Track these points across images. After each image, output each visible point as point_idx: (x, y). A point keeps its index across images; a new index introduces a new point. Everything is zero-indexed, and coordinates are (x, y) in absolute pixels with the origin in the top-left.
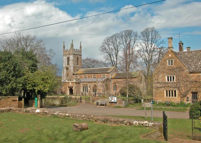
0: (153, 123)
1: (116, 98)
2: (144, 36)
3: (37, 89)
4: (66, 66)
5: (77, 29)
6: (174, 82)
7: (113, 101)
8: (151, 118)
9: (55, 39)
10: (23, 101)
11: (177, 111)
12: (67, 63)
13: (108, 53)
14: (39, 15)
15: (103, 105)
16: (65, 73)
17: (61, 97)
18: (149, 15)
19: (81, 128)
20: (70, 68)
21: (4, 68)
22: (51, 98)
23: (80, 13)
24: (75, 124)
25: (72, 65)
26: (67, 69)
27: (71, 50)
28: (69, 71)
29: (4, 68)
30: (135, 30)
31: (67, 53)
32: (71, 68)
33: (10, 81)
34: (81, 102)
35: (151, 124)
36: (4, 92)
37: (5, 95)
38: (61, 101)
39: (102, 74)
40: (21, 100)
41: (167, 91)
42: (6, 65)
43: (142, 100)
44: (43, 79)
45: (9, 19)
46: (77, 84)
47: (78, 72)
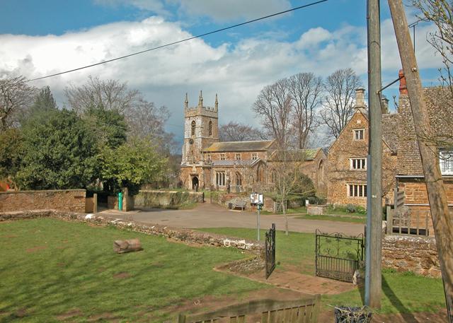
0: (252, 244)
1: (261, 196)
2: (333, 85)
3: (120, 178)
4: (190, 137)
5: (222, 71)
6: (363, 170)
7: (256, 201)
8: (257, 229)
9: (183, 90)
10: (95, 199)
11: (319, 219)
12: (190, 132)
13: (268, 114)
14: (154, 46)
15: (240, 209)
16: (188, 150)
17: (171, 192)
18: (352, 47)
19: (127, 248)
20: (196, 141)
21: (60, 139)
22: (155, 193)
23: (226, 42)
24: (117, 241)
25: (200, 136)
26: (191, 142)
27: (199, 109)
28: (194, 145)
29: (60, 139)
30: (317, 74)
31: (191, 114)
32: (198, 142)
33: (72, 162)
34: (204, 201)
35: (250, 245)
36: (60, 182)
37: (64, 187)
38: (171, 200)
39: (251, 153)
40: (92, 196)
41: (351, 186)
42: (64, 135)
43: (307, 202)
44: (132, 161)
45: (104, 51)
46: (207, 170)
47: (211, 149)
